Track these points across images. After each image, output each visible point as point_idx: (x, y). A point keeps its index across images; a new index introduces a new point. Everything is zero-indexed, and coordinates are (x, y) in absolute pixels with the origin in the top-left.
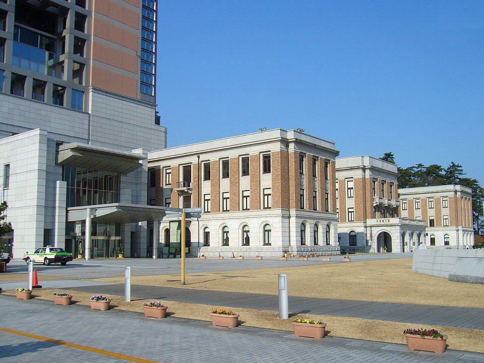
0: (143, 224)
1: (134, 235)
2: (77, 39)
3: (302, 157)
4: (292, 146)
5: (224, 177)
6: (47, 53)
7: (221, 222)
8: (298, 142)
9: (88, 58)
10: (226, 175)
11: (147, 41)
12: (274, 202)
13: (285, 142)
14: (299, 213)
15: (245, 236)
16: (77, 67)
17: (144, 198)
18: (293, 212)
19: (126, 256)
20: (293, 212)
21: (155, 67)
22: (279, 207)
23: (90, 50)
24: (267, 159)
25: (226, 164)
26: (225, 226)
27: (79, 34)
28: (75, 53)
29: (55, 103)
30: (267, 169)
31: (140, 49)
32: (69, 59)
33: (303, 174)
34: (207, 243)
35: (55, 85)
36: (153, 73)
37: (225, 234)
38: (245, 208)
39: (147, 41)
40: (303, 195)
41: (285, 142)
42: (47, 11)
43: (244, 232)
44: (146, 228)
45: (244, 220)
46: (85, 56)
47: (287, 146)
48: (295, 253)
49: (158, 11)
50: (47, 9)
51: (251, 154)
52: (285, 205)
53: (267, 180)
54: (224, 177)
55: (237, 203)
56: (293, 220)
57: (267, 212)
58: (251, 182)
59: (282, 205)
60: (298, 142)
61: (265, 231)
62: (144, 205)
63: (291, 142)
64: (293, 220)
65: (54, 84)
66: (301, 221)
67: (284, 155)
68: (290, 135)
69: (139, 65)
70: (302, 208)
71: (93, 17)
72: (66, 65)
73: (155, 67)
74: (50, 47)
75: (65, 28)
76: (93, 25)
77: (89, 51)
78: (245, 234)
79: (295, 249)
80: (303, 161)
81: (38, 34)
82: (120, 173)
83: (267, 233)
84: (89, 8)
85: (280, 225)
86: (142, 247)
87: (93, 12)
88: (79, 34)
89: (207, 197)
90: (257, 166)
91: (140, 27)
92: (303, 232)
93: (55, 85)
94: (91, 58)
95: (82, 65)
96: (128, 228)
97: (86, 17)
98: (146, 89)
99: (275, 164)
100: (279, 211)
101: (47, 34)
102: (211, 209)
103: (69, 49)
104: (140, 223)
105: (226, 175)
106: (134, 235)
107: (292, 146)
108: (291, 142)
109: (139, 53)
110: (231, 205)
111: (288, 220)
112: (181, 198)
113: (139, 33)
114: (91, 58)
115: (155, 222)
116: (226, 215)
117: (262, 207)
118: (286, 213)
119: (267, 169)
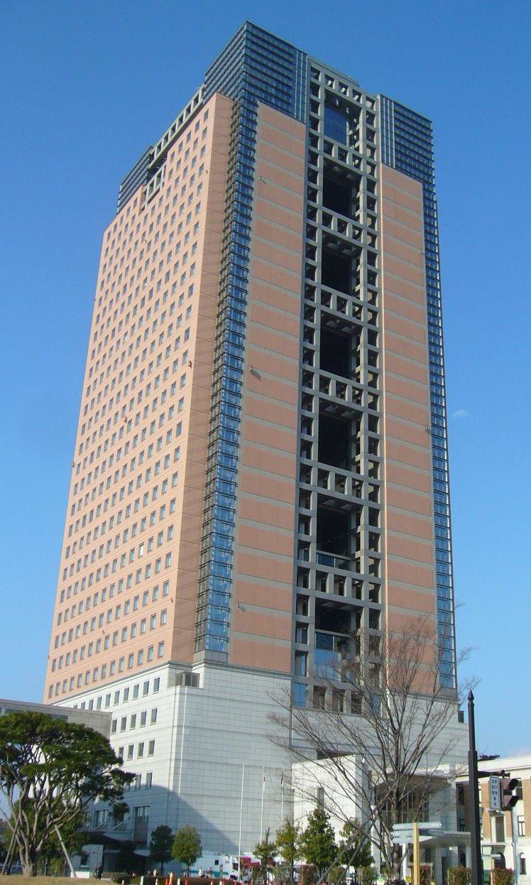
0: (454, 849)
1: (445, 862)
2: (371, 534)
9: (383, 579)
11: (439, 459)
16: (372, 562)
21: (450, 531)
27: (372, 434)
32: (365, 434)
34: (523, 872)
35: (354, 580)
39: (432, 316)
44: (457, 853)
46: (379, 551)
50: (343, 415)
62: (454, 831)
65: (353, 479)
69: (428, 378)
72: (362, 466)
73: (450, 531)
74: (342, 644)
77: (381, 342)
81: (333, 557)
82: (430, 792)
84: (379, 345)
87: (386, 530)
88: (373, 529)
89: (521, 819)
93: (354, 580)
94: (386, 528)
95: (377, 560)
96: (439, 854)
97: (379, 638)
98: (441, 509)
101: (341, 557)
102: (526, 833)
103: (364, 339)
104: (451, 849)
112: (493, 819)
114: (386, 528)
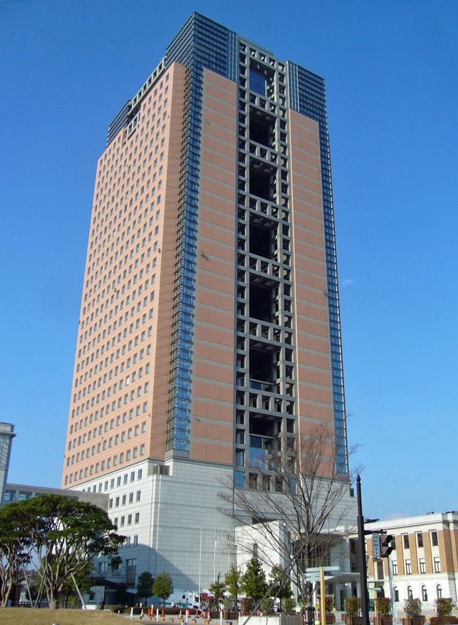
0: (349, 585)
1: (343, 593)
4: (452, 525)
5: (406, 548)
7: (407, 582)
9: (296, 397)
10: (407, 546)
11: (334, 329)
12: (442, 568)
13: (446, 522)
15: (424, 594)
21: (342, 363)
22: (445, 572)
23: (296, 373)
24: (435, 535)
25: (406, 538)
26: (409, 586)
27: (288, 363)
30: (435, 543)
31: (327, 290)
35: (275, 329)
39: (334, 329)
41: (446, 522)
43: (423, 590)
45: (422, 582)
47: (448, 525)
49: (344, 369)
53: (436, 551)
54: (406, 548)
55: (416, 569)
57: (438, 575)
58: (425, 552)
59: (448, 570)
61: (438, 590)
62: (348, 572)
67: (447, 532)
68: (450, 517)
69: (328, 316)
72: (281, 386)
73: (342, 363)
83: (439, 591)
84: (292, 295)
85: (447, 585)
86: (348, 593)
88: (288, 363)
90: (428, 540)
93: (275, 329)
94: (297, 362)
95: (291, 385)
96: (338, 588)
99: (441, 539)
100: (446, 575)
102: (399, 573)
104: (346, 584)
105: (407, 546)
106: (343, 593)
112: (376, 564)
113: (330, 373)
114: (297, 362)
116: (410, 577)
117: (434, 572)
118: (452, 576)
119: (435, 543)
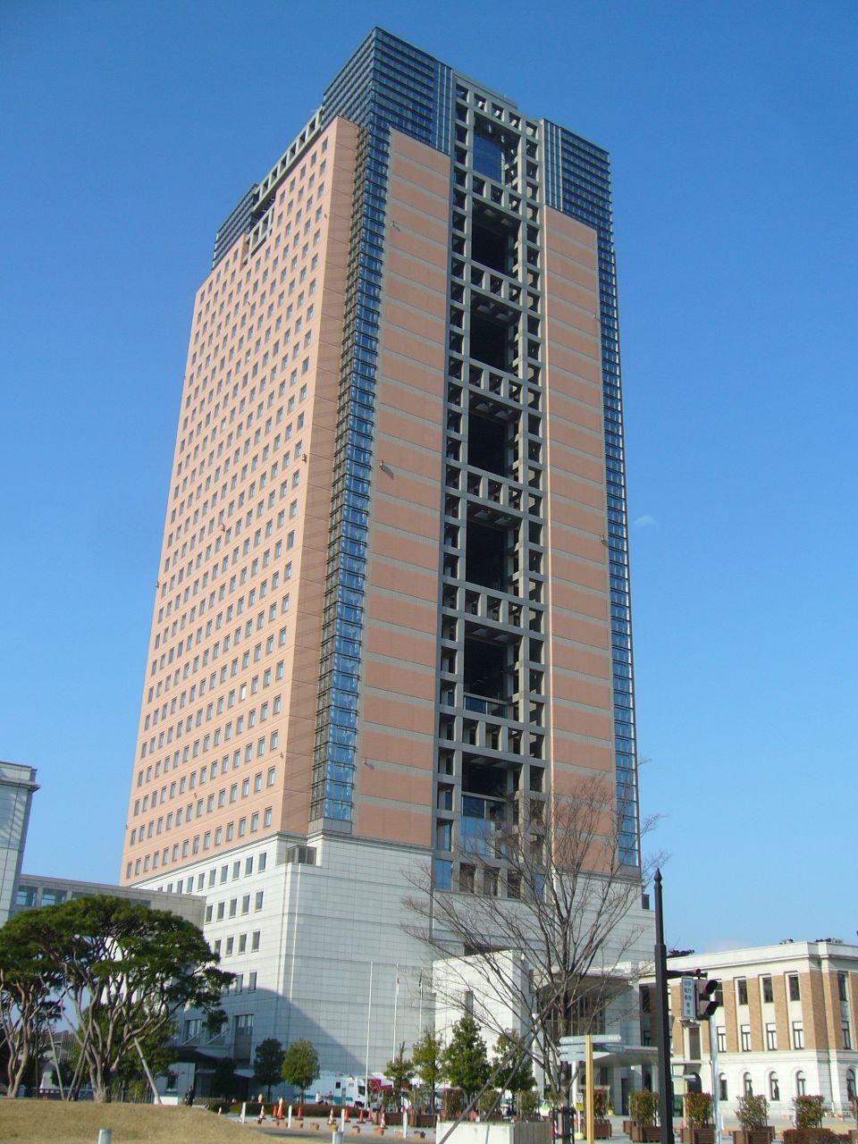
0: (637, 1069)
1: (626, 1084)
3: (841, 979)
5: (741, 1003)
6: (493, 825)
8: (832, 958)
9: (548, 728)
11: (617, 578)
12: (807, 1042)
13: (815, 959)
14: (841, 1056)
15: (774, 1087)
16: (533, 707)
17: (636, 1033)
18: (833, 1054)
19: (616, 1112)
20: (833, 1054)
21: (632, 668)
24: (794, 980)
25: (743, 986)
26: (747, 1073)
28: (531, 599)
29: (510, 895)
33: (845, 1000)
35: (511, 604)
36: (632, 722)
37: (748, 1084)
38: (771, 1047)
39: (617, 578)
40: (848, 1030)
41: (815, 959)
42: (498, 319)
43: (772, 1080)
45: (771, 1065)
47: (819, 964)
48: (840, 1112)
50: (497, 415)
51: (773, 974)
52: (822, 1044)
53: (796, 1010)
54: (741, 1003)
55: (759, 1041)
56: (834, 1065)
58: (777, 1011)
60: (832, 958)
62: (636, 1046)
63: (824, 959)
64: (834, 1065)
65: (510, 603)
66: (845, 1067)
67: (816, 977)
68: (823, 950)
70: (847, 1048)
71: (552, 736)
73: (632, 668)
75: (518, 789)
76: (552, 721)
78: (773, 1083)
79: (839, 1107)
80: (844, 981)
81: (485, 701)
82: (606, 996)
83: (801, 1083)
84: (545, 601)
85: (816, 1072)
86: (636, 1084)
87: (548, 389)
88: (535, 666)
90: (782, 990)
91: (601, 359)
92: (852, 1083)
94: (551, 664)
95: (540, 705)
96: (617, 1074)
99: (805, 988)
100: (813, 1054)
103: (524, 565)
104: (632, 1068)
106: (626, 1084)
107: (825, 965)
108: (824, 959)
109: (607, 539)
110: (753, 1043)
111: (826, 1066)
112: (686, 1031)
114: (551, 664)
115: (653, 1067)
117: (792, 1047)
118: (824, 1056)
